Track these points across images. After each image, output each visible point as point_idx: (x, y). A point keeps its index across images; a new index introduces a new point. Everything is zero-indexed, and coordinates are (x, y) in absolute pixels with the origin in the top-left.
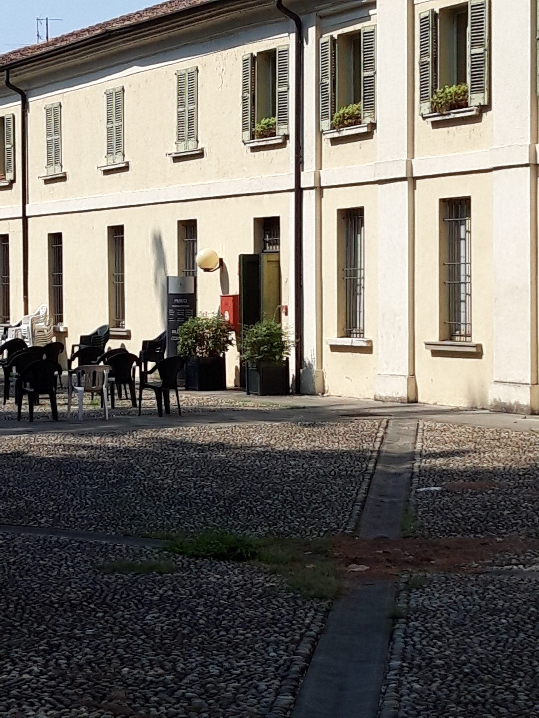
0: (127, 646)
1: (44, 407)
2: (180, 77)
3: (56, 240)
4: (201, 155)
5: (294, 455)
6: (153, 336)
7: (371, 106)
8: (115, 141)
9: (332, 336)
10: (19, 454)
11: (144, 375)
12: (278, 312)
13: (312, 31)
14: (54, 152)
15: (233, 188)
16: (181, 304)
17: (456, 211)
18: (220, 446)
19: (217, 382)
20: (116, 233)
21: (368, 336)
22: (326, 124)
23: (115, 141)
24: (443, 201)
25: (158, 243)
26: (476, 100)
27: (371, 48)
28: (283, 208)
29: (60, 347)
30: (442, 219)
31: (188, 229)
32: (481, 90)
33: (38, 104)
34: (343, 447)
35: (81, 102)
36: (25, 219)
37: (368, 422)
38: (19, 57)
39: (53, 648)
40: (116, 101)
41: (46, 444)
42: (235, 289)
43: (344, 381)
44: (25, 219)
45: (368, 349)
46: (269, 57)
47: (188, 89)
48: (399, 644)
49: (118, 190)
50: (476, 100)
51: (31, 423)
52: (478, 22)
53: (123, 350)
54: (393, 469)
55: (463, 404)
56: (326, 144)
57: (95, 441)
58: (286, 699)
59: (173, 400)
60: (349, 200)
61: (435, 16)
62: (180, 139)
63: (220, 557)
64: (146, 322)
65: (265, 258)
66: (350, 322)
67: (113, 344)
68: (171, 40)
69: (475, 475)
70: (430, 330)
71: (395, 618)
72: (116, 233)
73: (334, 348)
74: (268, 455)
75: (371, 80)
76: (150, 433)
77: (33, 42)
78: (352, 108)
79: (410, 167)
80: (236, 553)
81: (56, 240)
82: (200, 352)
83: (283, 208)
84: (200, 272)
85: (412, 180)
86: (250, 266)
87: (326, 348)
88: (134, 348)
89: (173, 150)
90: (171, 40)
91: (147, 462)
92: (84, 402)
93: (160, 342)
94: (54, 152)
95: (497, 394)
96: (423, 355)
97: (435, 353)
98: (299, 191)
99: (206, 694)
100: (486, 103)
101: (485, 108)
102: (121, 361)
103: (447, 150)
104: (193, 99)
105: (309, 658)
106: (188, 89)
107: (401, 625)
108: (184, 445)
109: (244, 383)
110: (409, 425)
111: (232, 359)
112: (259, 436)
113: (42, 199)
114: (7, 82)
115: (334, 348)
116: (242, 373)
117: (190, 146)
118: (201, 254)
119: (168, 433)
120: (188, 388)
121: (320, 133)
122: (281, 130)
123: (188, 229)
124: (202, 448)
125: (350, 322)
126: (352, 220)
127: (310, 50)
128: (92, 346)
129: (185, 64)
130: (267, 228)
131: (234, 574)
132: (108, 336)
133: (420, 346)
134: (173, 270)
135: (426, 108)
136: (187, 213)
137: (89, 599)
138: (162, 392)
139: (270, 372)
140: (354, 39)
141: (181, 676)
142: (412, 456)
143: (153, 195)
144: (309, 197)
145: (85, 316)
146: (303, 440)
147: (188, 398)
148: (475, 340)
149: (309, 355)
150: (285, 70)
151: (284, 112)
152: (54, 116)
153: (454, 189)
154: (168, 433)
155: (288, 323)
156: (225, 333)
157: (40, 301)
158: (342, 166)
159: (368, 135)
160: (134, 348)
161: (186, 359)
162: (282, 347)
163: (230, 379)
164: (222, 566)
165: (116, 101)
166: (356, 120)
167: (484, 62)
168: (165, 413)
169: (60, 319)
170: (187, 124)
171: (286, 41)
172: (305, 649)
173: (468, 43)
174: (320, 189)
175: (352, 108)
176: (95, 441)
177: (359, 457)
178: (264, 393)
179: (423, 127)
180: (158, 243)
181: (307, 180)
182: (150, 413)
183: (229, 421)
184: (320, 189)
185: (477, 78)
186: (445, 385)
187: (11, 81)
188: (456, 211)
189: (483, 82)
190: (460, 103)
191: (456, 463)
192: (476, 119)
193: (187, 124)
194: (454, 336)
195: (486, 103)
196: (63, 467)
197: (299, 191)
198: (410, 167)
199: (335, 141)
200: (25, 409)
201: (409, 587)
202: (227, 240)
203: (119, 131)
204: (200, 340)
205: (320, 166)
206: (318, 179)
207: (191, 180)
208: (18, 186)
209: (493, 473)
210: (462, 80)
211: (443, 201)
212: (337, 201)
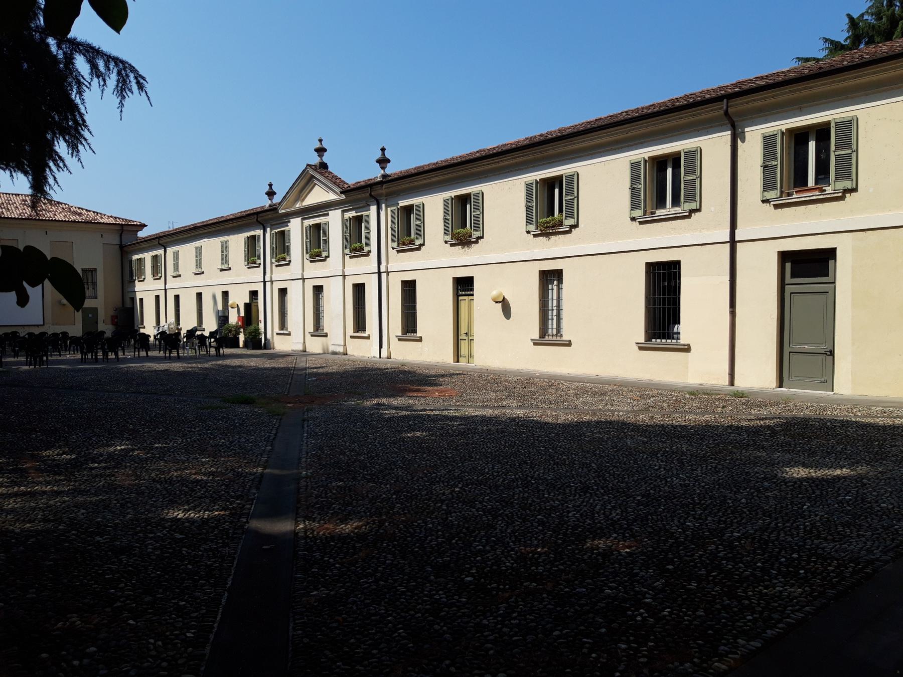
0: (211, 434)
1: (174, 354)
2: (222, 243)
3: (177, 297)
4: (230, 269)
5: (266, 369)
6: (213, 330)
7: (289, 254)
8: (199, 264)
9: (277, 330)
10: (166, 370)
11: (210, 343)
12: (258, 322)
13: (268, 229)
14: (176, 267)
15: (241, 281)
16: (223, 319)
17: (318, 290)
18: (240, 366)
19: (237, 346)
20: (199, 295)
21: (419, 334)
22: (274, 260)
23: (199, 264)
24: (402, 282)
25: (214, 297)
26: (324, 254)
27: (289, 236)
28: (259, 288)
29: (179, 334)
30: (540, 280)
31: (225, 294)
32: (572, 216)
33: (170, 251)
34: (282, 366)
35: (187, 251)
36: (166, 290)
37: (290, 358)
38: (468, 158)
39: (184, 435)
40: (199, 251)
41: (177, 366)
42: (242, 314)
43: (281, 345)
44: (166, 290)
45: (289, 334)
46: (254, 237)
47: (225, 247)
48: (306, 428)
49: (200, 281)
50: (324, 254)
51: (170, 359)
52: (325, 230)
53: (202, 335)
54: (300, 373)
55: (321, 352)
56: (347, 258)
57: (194, 365)
58: (269, 448)
59: (221, 351)
60: (282, 285)
61: (452, 199)
62: (222, 263)
63: (242, 403)
64: (210, 325)
65: (253, 304)
66: (283, 324)
67: (198, 333)
68: (219, 230)
69: (327, 374)
70: (310, 328)
71: (304, 420)
72: (199, 295)
73: (352, 337)
74: (257, 369)
75: (289, 247)
76: (214, 363)
77: (167, 229)
78: (282, 255)
79: (344, 272)
80: (248, 402)
81: (177, 297)
82: (230, 335)
83: (259, 288)
84: (230, 309)
85: (304, 279)
86: (248, 307)
87: (348, 338)
88: (207, 334)
89: (220, 267)
90: (617, 142)
91: (214, 372)
92: (188, 352)
93: (216, 332)
94: (176, 267)
95: (332, 349)
96: (308, 336)
97: (399, 340)
98: (265, 282)
99: (241, 448)
100: (854, 186)
101: (328, 257)
102: (202, 338)
103: (315, 270)
104: (227, 250)
105: (276, 435)
106: (225, 247)
107: (306, 423)
108: (226, 366)
109: (246, 345)
110: (304, 359)
111: (242, 337)
112: (253, 363)
113: (172, 283)
114: (371, 195)
115: (352, 337)
116: (245, 342)
117: (226, 266)
118: (230, 302)
119: (220, 362)
120: (226, 347)
121: (272, 263)
122: (258, 262)
123: (225, 294)
124: (233, 367)
125: (283, 324)
126: (283, 292)
127: (383, 213)
128: (191, 333)
129: (224, 239)
130: (254, 294)
131: (248, 409)
132: (197, 330)
133: (307, 333)
134: (220, 307)
135: (308, 256)
136: (225, 289)
137: (196, 418)
138: (217, 349)
139: (255, 342)
140: (283, 233)
141: (231, 443)
142: (305, 369)
143: (213, 282)
144: (268, 285)
145: (188, 323)
146: (268, 364)
147: (227, 351)
148: (325, 331)
149: (269, 336)
150: (259, 242)
151: (259, 255)
152: (176, 255)
153: (318, 283)
154: (220, 362)
155: (261, 326)
156: (239, 329)
157: (172, 318)
158: (279, 274)
159: (288, 264)
160: (207, 334)
161: (225, 337)
162: (260, 334)
163: (241, 344)
164: (243, 406)
165: (199, 251)
166: (284, 259)
167: (327, 242)
168: (218, 356)
169: (179, 324)
170: (225, 259)
171: (259, 232)
172: (274, 432)
173: (833, 147)
174: (272, 282)
175: (282, 255)
176: (194, 365)
177: (287, 369)
178: (253, 349)
179: (307, 262)
180: (214, 297)
181: (383, 269)
182: (213, 356)
183: (241, 358)
184: (272, 282)
185: (325, 247)
186: (315, 346)
187: (730, 110)
188: (318, 290)
189: (326, 248)
190: (319, 255)
191: (321, 370)
192: (324, 260)
193: (225, 259)
194: (318, 330)
195: (854, 186)
196: (183, 374)
197: (265, 282)
198: (344, 272)
199: (277, 266)
200: (167, 355)
201: (308, 410)
202: (239, 298)
203: (200, 260)
204: (230, 331)
205: (272, 273)
206: (387, 268)
207: (226, 278)
208: (163, 278)
209: (332, 373)
210: (319, 247)
211: (402, 282)
212: (277, 286)
